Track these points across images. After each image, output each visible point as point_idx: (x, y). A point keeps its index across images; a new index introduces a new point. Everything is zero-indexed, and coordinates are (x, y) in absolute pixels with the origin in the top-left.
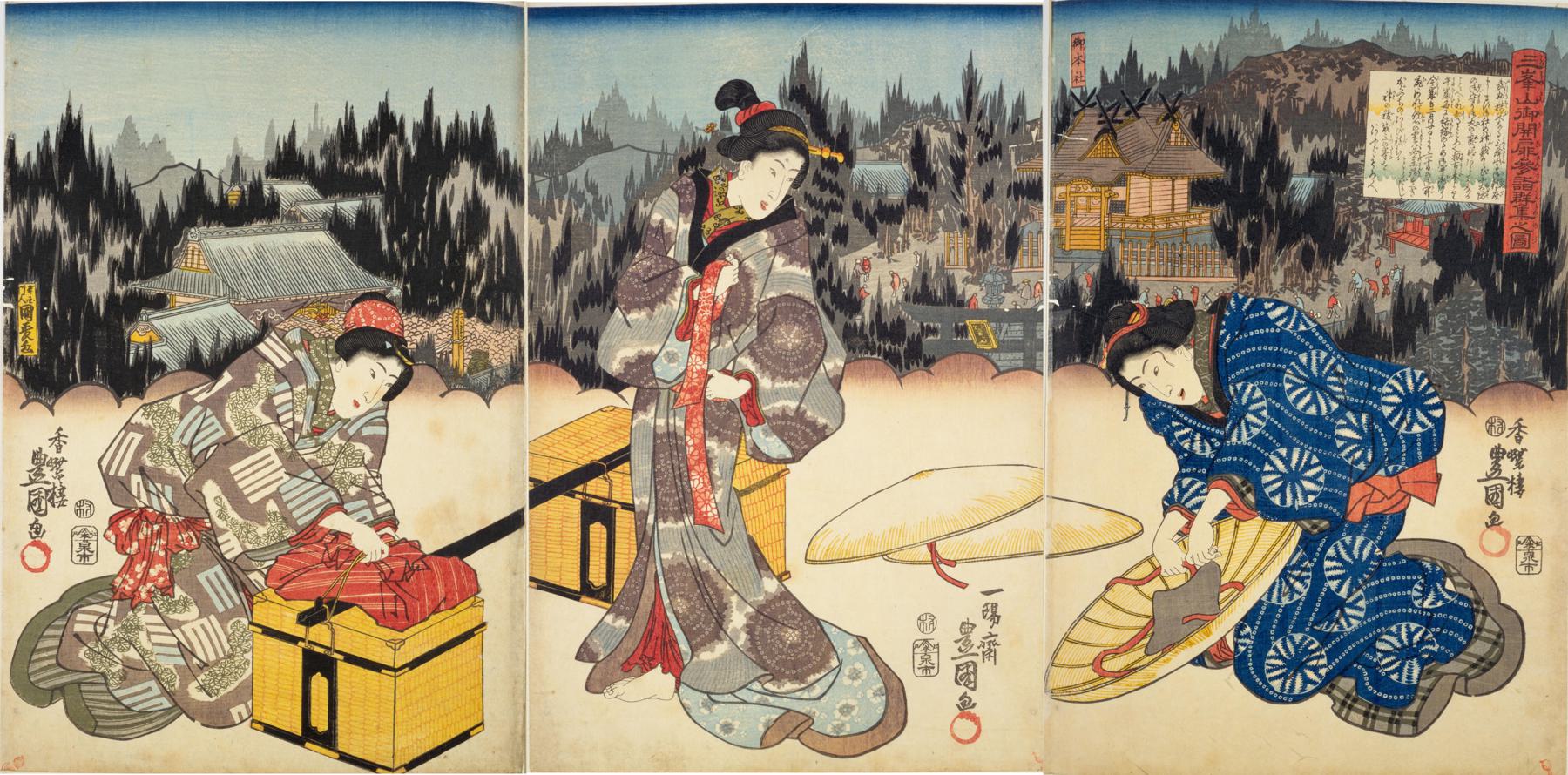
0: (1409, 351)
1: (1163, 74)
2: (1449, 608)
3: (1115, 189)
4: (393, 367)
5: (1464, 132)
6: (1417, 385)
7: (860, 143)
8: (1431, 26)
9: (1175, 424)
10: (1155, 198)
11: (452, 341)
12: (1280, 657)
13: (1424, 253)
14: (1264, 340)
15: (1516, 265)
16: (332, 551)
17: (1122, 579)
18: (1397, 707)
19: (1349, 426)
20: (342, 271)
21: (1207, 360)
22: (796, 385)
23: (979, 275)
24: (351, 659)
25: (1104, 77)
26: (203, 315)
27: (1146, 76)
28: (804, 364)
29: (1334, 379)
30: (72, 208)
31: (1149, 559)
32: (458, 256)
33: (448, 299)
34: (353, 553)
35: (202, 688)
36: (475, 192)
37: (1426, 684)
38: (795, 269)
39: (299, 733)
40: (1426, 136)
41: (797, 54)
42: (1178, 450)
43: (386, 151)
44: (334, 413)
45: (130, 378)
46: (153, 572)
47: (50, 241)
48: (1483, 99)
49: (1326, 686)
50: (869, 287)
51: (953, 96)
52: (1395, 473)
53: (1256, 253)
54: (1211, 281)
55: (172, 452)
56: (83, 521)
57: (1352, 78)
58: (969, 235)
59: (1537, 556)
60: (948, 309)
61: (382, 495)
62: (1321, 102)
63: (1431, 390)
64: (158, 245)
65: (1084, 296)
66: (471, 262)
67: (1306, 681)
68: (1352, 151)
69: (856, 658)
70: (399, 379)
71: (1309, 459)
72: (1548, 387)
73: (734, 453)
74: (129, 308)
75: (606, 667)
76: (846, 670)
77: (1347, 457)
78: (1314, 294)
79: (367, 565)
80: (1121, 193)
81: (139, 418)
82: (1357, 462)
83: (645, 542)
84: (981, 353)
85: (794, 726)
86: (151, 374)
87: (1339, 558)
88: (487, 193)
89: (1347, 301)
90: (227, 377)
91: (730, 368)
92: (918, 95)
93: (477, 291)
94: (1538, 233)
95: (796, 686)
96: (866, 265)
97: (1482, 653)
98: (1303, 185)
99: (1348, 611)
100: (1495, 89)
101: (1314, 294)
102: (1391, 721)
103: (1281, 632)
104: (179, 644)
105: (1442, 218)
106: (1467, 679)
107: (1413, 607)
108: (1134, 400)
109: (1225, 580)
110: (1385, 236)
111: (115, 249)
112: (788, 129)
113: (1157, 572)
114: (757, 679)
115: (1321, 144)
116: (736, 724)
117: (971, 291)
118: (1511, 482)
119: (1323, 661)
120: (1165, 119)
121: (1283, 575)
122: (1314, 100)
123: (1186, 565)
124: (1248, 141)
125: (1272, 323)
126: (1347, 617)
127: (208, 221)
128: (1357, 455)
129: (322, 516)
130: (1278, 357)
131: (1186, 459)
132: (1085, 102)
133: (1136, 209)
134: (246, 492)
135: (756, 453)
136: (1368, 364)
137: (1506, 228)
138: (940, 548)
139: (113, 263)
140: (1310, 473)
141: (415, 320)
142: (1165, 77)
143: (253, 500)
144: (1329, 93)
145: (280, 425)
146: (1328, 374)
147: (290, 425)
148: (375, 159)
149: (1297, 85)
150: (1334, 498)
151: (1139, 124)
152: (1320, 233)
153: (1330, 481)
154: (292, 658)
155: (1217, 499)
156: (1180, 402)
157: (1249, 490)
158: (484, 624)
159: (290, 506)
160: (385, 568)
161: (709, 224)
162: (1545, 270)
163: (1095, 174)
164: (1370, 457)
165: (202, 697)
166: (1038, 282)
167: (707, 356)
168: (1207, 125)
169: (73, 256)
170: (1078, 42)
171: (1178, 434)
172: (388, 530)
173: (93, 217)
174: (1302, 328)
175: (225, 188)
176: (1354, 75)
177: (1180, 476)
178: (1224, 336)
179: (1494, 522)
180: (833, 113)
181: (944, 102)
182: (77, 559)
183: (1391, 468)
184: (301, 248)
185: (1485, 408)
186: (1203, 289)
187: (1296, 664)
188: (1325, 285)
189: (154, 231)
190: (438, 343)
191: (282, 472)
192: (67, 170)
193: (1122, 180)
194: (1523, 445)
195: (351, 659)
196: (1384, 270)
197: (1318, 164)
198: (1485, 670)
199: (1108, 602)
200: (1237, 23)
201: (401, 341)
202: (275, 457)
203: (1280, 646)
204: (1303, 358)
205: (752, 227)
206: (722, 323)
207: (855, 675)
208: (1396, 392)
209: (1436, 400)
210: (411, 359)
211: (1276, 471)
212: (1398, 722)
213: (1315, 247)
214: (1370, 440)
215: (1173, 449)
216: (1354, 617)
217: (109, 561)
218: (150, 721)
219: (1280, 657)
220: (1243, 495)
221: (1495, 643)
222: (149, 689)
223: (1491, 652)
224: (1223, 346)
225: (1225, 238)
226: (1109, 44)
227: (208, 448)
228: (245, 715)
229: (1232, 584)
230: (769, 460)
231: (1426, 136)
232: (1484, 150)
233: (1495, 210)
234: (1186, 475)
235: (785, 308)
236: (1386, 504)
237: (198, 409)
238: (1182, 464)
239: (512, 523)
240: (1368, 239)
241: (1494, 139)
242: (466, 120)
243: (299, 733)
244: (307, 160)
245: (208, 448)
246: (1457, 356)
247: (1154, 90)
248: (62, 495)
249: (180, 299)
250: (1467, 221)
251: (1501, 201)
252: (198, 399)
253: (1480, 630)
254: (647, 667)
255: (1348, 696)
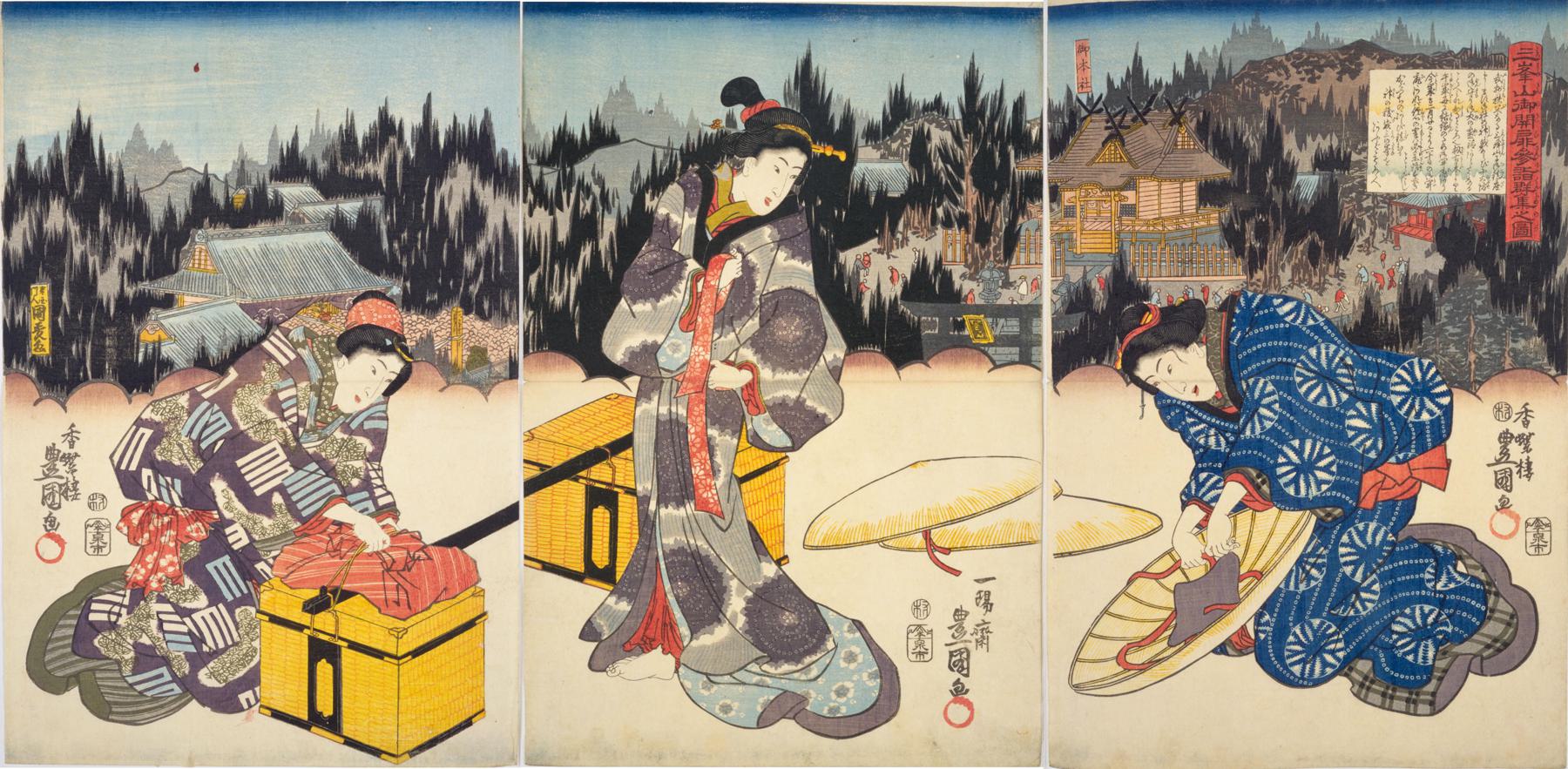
0: (1416, 341)
1: (1168, 79)
2: (1461, 590)
3: (1124, 193)
4: (394, 364)
5: (1463, 125)
6: (1424, 374)
7: (862, 142)
8: (1429, 23)
9: (1190, 420)
10: (1166, 201)
11: (451, 338)
12: (1300, 643)
13: (1429, 245)
14: (1274, 335)
15: (1518, 254)
16: (336, 541)
17: (1143, 574)
18: (1414, 687)
19: (1360, 416)
20: (341, 271)
21: (1220, 356)
22: (796, 376)
23: (977, 271)
24: (353, 646)
25: (1110, 83)
26: (210, 314)
27: (1151, 83)
28: (803, 355)
29: (1344, 371)
30: (84, 213)
31: (1169, 553)
32: (456, 258)
33: (446, 297)
34: (356, 543)
35: (212, 674)
36: (473, 194)
37: (1441, 664)
38: (796, 263)
39: (305, 717)
40: (1426, 132)
41: (802, 56)
42: (1193, 446)
43: (386, 155)
44: (336, 409)
45: (139, 376)
46: (163, 563)
47: (60, 245)
48: (1480, 93)
49: (1345, 668)
50: (869, 281)
51: (954, 97)
52: (1405, 461)
53: (1264, 252)
54: (1223, 282)
55: (180, 446)
56: (96, 514)
57: (1353, 78)
58: (967, 232)
59: (1547, 537)
60: (946, 307)
61: (383, 486)
62: (1323, 100)
63: (1439, 378)
64: (166, 248)
65: (1097, 298)
66: (469, 261)
67: (1325, 664)
68: (1355, 147)
69: (853, 642)
70: (399, 376)
71: (1322, 449)
72: (1553, 372)
73: (735, 441)
74: (140, 307)
75: (607, 647)
76: (842, 653)
77: (1358, 446)
78: (1321, 289)
79: (370, 555)
80: (1130, 196)
81: (147, 415)
82: (1367, 451)
83: (647, 525)
84: (977, 347)
85: (789, 707)
86: (160, 371)
87: (1352, 544)
88: (486, 194)
89: (1353, 296)
90: (233, 374)
91: (732, 358)
92: (919, 94)
93: (474, 289)
94: (1539, 222)
95: (793, 668)
96: (865, 262)
97: (1497, 634)
98: (1308, 183)
99: (1364, 595)
100: (1493, 83)
101: (1321, 289)
102: (1408, 700)
103: (1300, 619)
104: (190, 633)
105: (1445, 211)
106: (1483, 659)
107: (1426, 589)
108: (1149, 398)
109: (1243, 570)
110: (1390, 230)
111: (125, 251)
112: (792, 128)
113: (1177, 566)
114: (756, 660)
115: (1325, 143)
116: (735, 705)
117: (967, 286)
118: (1520, 466)
119: (1340, 645)
120: (1171, 124)
121: (1300, 562)
122: (1316, 100)
123: (1205, 556)
124: (1253, 142)
125: (1281, 319)
126: (1363, 601)
127: (213, 223)
128: (1369, 443)
129: (325, 507)
130: (1288, 352)
131: (1202, 455)
132: (1092, 109)
133: (1147, 212)
134: (252, 485)
135: (757, 442)
136: (1376, 356)
137: (1507, 219)
138: (935, 535)
139: (124, 265)
140: (1322, 464)
141: (415, 317)
142: (1170, 81)
143: (258, 492)
144: (1331, 93)
145: (284, 419)
146: (1338, 366)
147: (294, 419)
148: (375, 160)
149: (1299, 87)
150: (1348, 484)
151: (1147, 129)
152: (1326, 230)
153: (1342, 470)
154: (300, 642)
155: (1234, 492)
156: (1194, 398)
157: (1263, 482)
158: (484, 614)
159: (294, 498)
160: (387, 558)
161: (713, 222)
162: (1549, 259)
163: (1105, 180)
164: (1380, 446)
165: (212, 683)
166: (1039, 280)
167: (711, 347)
168: (1212, 127)
169: (84, 257)
170: (1082, 49)
171: (1193, 430)
172: (389, 521)
173: (103, 219)
174: (1311, 322)
175: (231, 191)
176: (1354, 74)
177: (1195, 473)
178: (1235, 333)
179: (1504, 506)
180: (836, 112)
181: (945, 101)
182: (90, 551)
183: (1401, 456)
184: (301, 249)
185: (1492, 393)
186: (1213, 288)
187: (1315, 650)
188: (1332, 280)
189: (162, 234)
190: (437, 339)
191: (287, 466)
192: (77, 174)
193: (1130, 184)
194: (1531, 429)
195: (353, 646)
196: (1389, 263)
197: (1320, 163)
198: (1499, 651)
199: (1129, 596)
200: (1240, 28)
201: (402, 339)
202: (280, 451)
203: (1298, 632)
204: (1313, 352)
205: (751, 223)
206: (726, 318)
207: (851, 658)
208: (1404, 381)
209: (1443, 388)
210: (410, 356)
211: (1289, 463)
212: (1415, 702)
213: (1321, 244)
214: (1381, 429)
215: (1189, 445)
216: (1370, 601)
217: (121, 552)
218: (162, 707)
219: (1300, 643)
220: (1258, 488)
221: (1509, 624)
222: (161, 676)
223: (1505, 632)
224: (1235, 343)
225: (1232, 237)
226: (1114, 51)
227: (215, 443)
228: (253, 701)
229: (1251, 573)
230: (771, 449)
231: (1426, 132)
232: (1483, 143)
233: (1497, 200)
234: (1203, 470)
235: (784, 301)
236: (1398, 490)
237: (205, 404)
238: (1198, 459)
239: (508, 515)
240: (1373, 233)
241: (1493, 131)
242: (464, 122)
243: (305, 717)
244: (309, 163)
245: (215, 443)
246: (1465, 345)
247: (1160, 94)
248: (75, 489)
249: (188, 300)
250: (1469, 213)
251: (1502, 191)
252: (206, 395)
253: (1492, 611)
254: (646, 646)
255: (1366, 678)
